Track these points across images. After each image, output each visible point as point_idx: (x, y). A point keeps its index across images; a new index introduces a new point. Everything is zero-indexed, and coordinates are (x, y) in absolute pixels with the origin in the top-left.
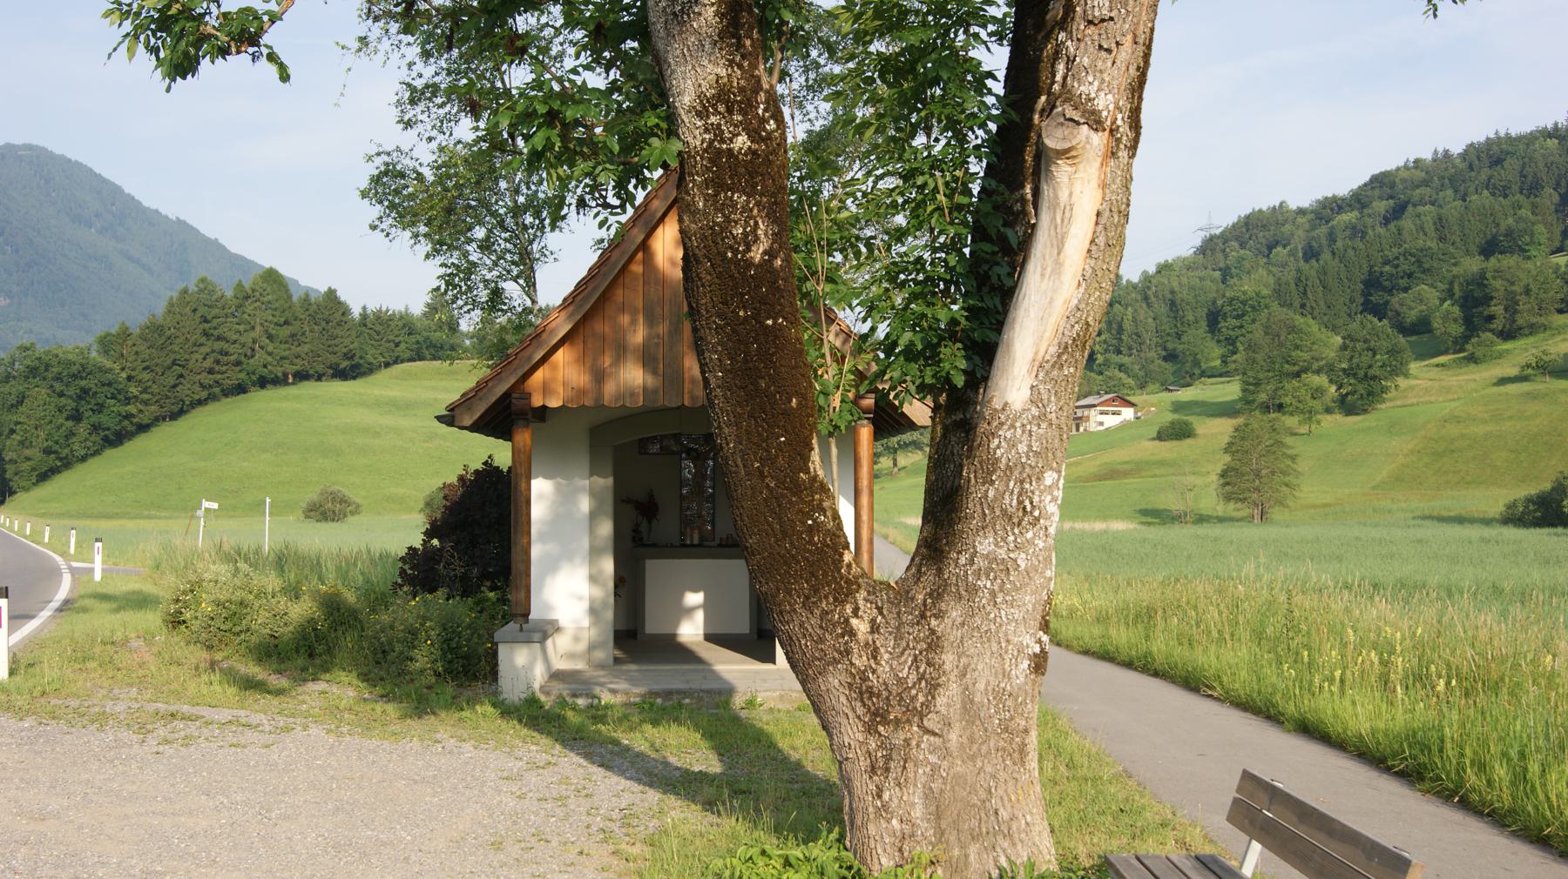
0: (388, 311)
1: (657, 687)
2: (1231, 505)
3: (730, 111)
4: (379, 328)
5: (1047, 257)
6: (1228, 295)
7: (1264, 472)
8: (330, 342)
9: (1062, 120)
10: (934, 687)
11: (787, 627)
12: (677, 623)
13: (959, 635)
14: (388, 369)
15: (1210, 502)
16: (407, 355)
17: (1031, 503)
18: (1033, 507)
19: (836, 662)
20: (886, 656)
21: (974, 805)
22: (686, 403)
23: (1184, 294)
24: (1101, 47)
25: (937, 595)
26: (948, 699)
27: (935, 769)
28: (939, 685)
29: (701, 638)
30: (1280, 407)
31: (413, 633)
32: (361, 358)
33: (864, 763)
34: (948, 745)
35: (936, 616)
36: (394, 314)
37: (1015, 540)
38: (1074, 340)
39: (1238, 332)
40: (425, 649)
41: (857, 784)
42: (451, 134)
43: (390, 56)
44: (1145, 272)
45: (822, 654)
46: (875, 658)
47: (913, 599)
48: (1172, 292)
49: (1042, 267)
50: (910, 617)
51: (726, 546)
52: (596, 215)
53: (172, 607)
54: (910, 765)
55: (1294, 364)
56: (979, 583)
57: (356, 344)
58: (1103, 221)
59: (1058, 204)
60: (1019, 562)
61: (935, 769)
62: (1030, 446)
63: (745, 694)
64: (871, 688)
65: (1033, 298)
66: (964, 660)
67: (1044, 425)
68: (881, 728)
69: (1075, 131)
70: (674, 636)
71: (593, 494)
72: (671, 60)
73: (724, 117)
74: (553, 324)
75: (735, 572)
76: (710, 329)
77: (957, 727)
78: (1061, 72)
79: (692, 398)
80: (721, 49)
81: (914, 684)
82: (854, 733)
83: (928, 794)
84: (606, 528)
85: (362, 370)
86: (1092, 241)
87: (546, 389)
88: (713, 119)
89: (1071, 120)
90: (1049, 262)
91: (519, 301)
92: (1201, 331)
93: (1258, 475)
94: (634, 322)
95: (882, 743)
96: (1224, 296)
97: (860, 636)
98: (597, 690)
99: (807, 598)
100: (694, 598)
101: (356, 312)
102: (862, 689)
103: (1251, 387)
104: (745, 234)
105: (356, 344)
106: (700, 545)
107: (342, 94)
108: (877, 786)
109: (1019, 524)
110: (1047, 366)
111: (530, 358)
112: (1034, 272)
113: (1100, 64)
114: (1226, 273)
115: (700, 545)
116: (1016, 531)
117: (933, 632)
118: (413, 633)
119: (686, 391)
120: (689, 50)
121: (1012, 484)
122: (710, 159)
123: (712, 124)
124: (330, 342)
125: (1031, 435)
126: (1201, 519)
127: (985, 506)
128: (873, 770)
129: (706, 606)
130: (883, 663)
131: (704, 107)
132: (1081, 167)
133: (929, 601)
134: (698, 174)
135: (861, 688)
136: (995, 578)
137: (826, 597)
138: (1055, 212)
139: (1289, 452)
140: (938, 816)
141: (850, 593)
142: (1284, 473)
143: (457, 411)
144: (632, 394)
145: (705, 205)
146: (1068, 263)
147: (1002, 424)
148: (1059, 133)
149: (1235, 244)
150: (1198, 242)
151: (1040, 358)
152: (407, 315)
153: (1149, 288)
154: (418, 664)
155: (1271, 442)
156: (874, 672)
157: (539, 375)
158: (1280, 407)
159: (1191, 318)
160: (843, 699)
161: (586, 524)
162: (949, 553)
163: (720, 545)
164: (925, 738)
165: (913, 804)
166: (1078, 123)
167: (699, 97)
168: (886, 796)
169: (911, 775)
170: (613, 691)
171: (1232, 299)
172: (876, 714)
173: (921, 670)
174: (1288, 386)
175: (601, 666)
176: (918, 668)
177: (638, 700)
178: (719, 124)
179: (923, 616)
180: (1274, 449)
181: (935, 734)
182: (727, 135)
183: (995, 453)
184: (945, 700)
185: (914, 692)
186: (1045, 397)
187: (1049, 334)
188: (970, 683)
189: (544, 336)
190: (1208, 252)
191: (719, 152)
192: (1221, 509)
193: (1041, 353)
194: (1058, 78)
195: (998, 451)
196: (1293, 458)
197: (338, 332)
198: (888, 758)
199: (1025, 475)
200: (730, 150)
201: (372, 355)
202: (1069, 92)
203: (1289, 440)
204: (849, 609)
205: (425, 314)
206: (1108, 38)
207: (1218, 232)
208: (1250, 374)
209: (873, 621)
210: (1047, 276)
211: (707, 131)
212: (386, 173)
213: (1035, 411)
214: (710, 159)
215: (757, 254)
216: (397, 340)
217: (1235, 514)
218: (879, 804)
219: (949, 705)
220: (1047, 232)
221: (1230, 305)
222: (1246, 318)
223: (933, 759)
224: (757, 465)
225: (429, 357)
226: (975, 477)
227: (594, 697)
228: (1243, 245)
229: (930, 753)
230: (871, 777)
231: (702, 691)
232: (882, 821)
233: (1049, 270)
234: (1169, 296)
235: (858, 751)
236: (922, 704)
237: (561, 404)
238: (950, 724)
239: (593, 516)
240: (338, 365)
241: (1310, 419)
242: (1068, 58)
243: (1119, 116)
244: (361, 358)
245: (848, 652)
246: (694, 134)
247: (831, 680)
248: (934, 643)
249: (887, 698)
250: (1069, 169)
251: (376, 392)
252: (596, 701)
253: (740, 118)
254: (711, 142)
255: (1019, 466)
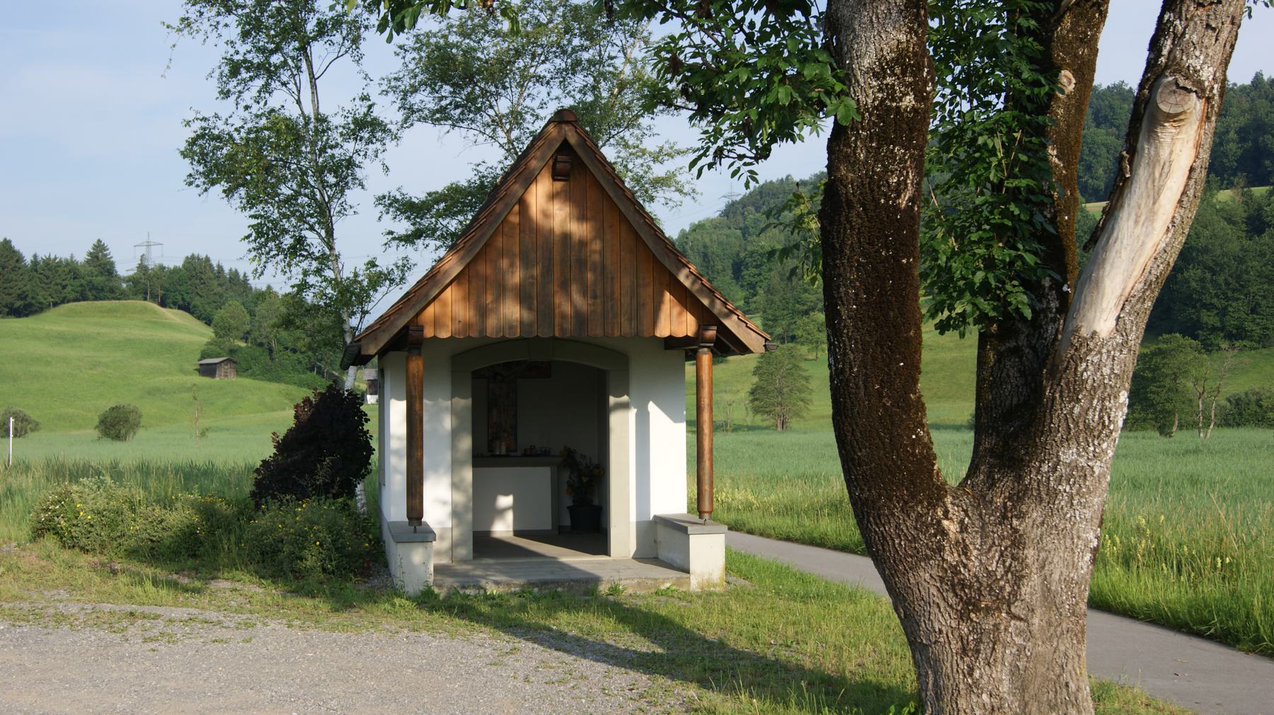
0: (56, 258)
1: (534, 578)
2: (759, 417)
3: (904, 73)
4: (48, 273)
5: (1143, 206)
6: (749, 249)
7: (785, 390)
8: (5, 285)
9: (1174, 88)
10: (1018, 579)
11: (882, 529)
12: (491, 523)
13: (1039, 533)
14: (57, 308)
15: (741, 414)
16: (73, 296)
17: (1109, 418)
18: (1110, 421)
19: (928, 558)
20: (975, 552)
21: (1051, 680)
22: (557, 334)
23: (714, 248)
24: (1208, 26)
25: (1018, 497)
26: (1031, 588)
27: (1021, 649)
28: (1024, 577)
29: (511, 534)
30: (793, 338)
31: (304, 535)
32: (33, 298)
33: (955, 646)
34: (1031, 628)
35: (1018, 518)
36: (61, 261)
37: (1094, 451)
38: (1157, 278)
39: (757, 279)
40: (315, 550)
41: (947, 666)
42: (266, 103)
43: (209, 34)
44: (683, 231)
45: (915, 551)
46: (965, 554)
47: (991, 502)
48: (705, 247)
49: (1136, 215)
50: (992, 518)
51: (530, 456)
52: (732, 164)
53: (42, 515)
54: (999, 648)
55: (804, 304)
56: (1060, 487)
57: (28, 287)
58: (1195, 175)
59: (1159, 161)
60: (1095, 469)
61: (1021, 649)
62: (1112, 369)
63: (608, 582)
64: (963, 580)
65: (1125, 241)
66: (1043, 555)
67: (1125, 351)
68: (973, 615)
69: (1187, 98)
70: (489, 532)
71: (454, 412)
72: (857, 27)
73: (898, 79)
74: (447, 266)
75: (540, 478)
76: (851, 267)
77: (1038, 612)
78: (1168, 47)
79: (562, 329)
80: (905, 17)
81: (1002, 576)
82: (946, 620)
83: (1014, 671)
84: (466, 443)
85: (34, 309)
86: (1184, 193)
87: (437, 323)
88: (889, 80)
89: (1184, 88)
90: (1144, 211)
91: (319, 248)
92: (727, 278)
93: (780, 392)
94: (512, 265)
95: (973, 628)
96: (746, 250)
97: (952, 535)
98: (483, 583)
99: (906, 503)
100: (505, 501)
101: (28, 259)
102: (954, 581)
103: (770, 323)
104: (898, 183)
105: (28, 287)
106: (507, 456)
107: (168, 67)
108: (968, 666)
109: (1099, 436)
110: (1134, 301)
111: (427, 295)
112: (1128, 219)
113: (1206, 41)
114: (745, 231)
115: (507, 456)
116: (1096, 443)
117: (1016, 531)
118: (304, 535)
119: (557, 323)
120: (877, 17)
121: (1095, 402)
122: (878, 115)
123: (887, 85)
124: (5, 285)
125: (1113, 360)
126: (737, 429)
127: (1070, 421)
128: (964, 651)
129: (515, 507)
130: (973, 558)
131: (883, 67)
132: (1184, 129)
133: (1009, 504)
134: (863, 129)
135: (952, 581)
136: (1075, 482)
137: (921, 502)
138: (1154, 167)
139: (805, 374)
140: (1024, 689)
141: (940, 499)
142: (800, 391)
143: (363, 342)
144: (511, 327)
145: (866, 157)
146: (1161, 211)
147: (1091, 350)
148: (1172, 99)
149: (752, 209)
150: (722, 207)
151: (1126, 294)
152: (72, 262)
153: (686, 243)
154: (308, 563)
155: (790, 366)
156: (965, 566)
157: (430, 311)
158: (793, 338)
159: (720, 267)
160: (933, 591)
161: (449, 440)
162: (1030, 461)
163: (524, 455)
164: (1012, 622)
165: (1001, 681)
166: (1190, 91)
167: (879, 60)
168: (977, 674)
169: (999, 656)
170: (497, 583)
171: (752, 252)
172: (967, 603)
173: (1007, 564)
174: (799, 322)
175: (464, 561)
176: (1004, 562)
177: (517, 589)
178: (893, 85)
179: (1004, 517)
180: (793, 371)
181: (1020, 619)
182: (898, 94)
183: (1082, 375)
184: (1029, 590)
185: (1002, 583)
186: (1128, 327)
187: (1137, 272)
188: (1048, 573)
189: (439, 276)
190: (731, 215)
191: (889, 109)
192: (749, 420)
193: (1128, 289)
194: (1165, 52)
195: (1085, 374)
196: (807, 379)
197: (12, 276)
198: (979, 641)
199: (1106, 394)
200: (898, 108)
201: (42, 296)
202: (1178, 64)
203: (803, 365)
204: (940, 513)
205: (88, 262)
206: (1216, 18)
207: (738, 198)
208: (769, 311)
209: (961, 522)
210: (1141, 223)
211: (880, 90)
212: (202, 136)
213: (1119, 339)
214: (878, 115)
215: (903, 202)
216: (64, 283)
217: (761, 424)
218: (970, 681)
219: (1031, 594)
220: (1143, 187)
221: (751, 257)
222: (764, 267)
223: (1019, 640)
224: (877, 387)
225: (91, 297)
226: (1061, 396)
227: (480, 588)
228: (757, 209)
229: (1017, 636)
230: (962, 658)
231: (572, 580)
232: (973, 696)
233: (1143, 218)
234: (702, 250)
235: (950, 635)
236: (1010, 593)
237: (449, 335)
238: (1033, 610)
239: (455, 433)
240: (13, 304)
241: (817, 348)
242: (1175, 35)
243: (1216, 86)
244: (33, 298)
245: (940, 549)
246: (867, 92)
247: (921, 574)
248: (1017, 541)
249: (979, 589)
250: (1174, 131)
251: (47, 327)
252: (482, 592)
253: (911, 80)
254: (883, 100)
255: (1102, 387)
